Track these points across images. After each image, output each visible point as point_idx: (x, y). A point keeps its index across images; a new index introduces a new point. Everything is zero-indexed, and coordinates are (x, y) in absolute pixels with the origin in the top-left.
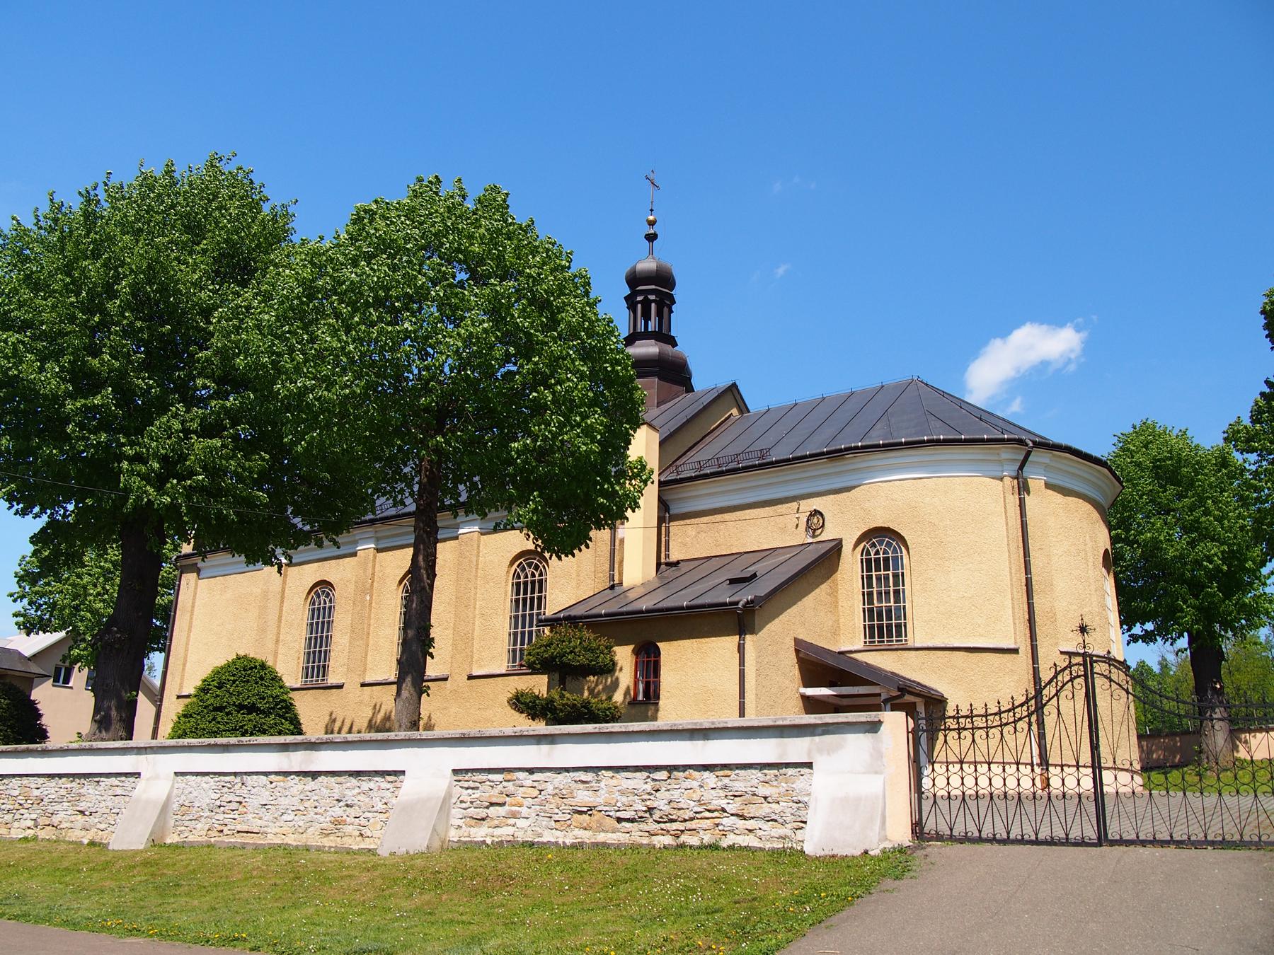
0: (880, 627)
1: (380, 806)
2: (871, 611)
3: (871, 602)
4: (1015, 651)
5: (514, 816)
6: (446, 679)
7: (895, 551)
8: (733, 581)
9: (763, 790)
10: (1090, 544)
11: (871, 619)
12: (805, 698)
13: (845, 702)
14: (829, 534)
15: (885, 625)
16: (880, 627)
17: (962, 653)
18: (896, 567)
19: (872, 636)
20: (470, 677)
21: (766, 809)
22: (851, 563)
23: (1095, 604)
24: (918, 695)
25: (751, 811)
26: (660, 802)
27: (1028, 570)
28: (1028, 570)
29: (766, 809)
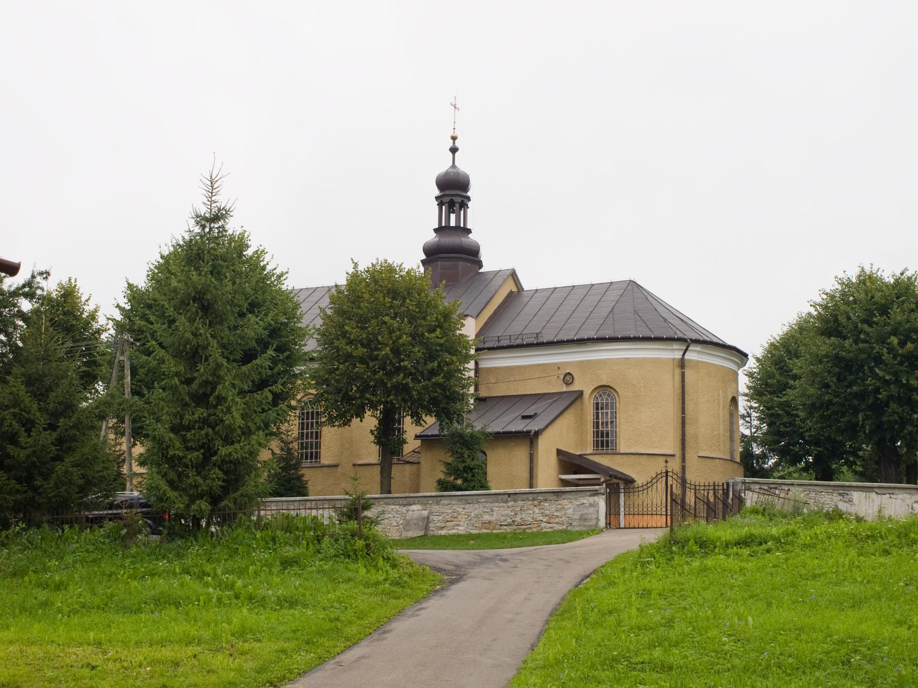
0: (602, 442)
1: (395, 524)
2: (597, 432)
3: (598, 427)
4: (673, 455)
5: (458, 525)
6: (336, 466)
7: (612, 399)
8: (524, 417)
9: (556, 514)
10: (721, 394)
11: (598, 437)
12: (562, 480)
13: (582, 482)
14: (575, 387)
15: (604, 440)
16: (602, 442)
17: (687, 427)
18: (612, 408)
19: (597, 446)
20: (354, 465)
21: (557, 520)
22: (588, 403)
23: (721, 430)
24: (620, 479)
25: (552, 520)
26: (518, 519)
27: (683, 412)
28: (683, 412)
29: (557, 520)
